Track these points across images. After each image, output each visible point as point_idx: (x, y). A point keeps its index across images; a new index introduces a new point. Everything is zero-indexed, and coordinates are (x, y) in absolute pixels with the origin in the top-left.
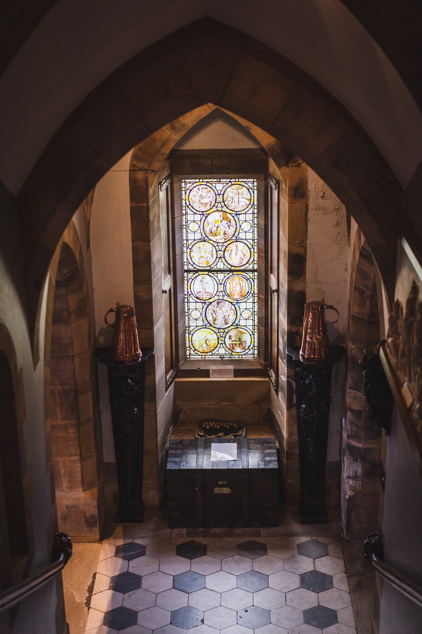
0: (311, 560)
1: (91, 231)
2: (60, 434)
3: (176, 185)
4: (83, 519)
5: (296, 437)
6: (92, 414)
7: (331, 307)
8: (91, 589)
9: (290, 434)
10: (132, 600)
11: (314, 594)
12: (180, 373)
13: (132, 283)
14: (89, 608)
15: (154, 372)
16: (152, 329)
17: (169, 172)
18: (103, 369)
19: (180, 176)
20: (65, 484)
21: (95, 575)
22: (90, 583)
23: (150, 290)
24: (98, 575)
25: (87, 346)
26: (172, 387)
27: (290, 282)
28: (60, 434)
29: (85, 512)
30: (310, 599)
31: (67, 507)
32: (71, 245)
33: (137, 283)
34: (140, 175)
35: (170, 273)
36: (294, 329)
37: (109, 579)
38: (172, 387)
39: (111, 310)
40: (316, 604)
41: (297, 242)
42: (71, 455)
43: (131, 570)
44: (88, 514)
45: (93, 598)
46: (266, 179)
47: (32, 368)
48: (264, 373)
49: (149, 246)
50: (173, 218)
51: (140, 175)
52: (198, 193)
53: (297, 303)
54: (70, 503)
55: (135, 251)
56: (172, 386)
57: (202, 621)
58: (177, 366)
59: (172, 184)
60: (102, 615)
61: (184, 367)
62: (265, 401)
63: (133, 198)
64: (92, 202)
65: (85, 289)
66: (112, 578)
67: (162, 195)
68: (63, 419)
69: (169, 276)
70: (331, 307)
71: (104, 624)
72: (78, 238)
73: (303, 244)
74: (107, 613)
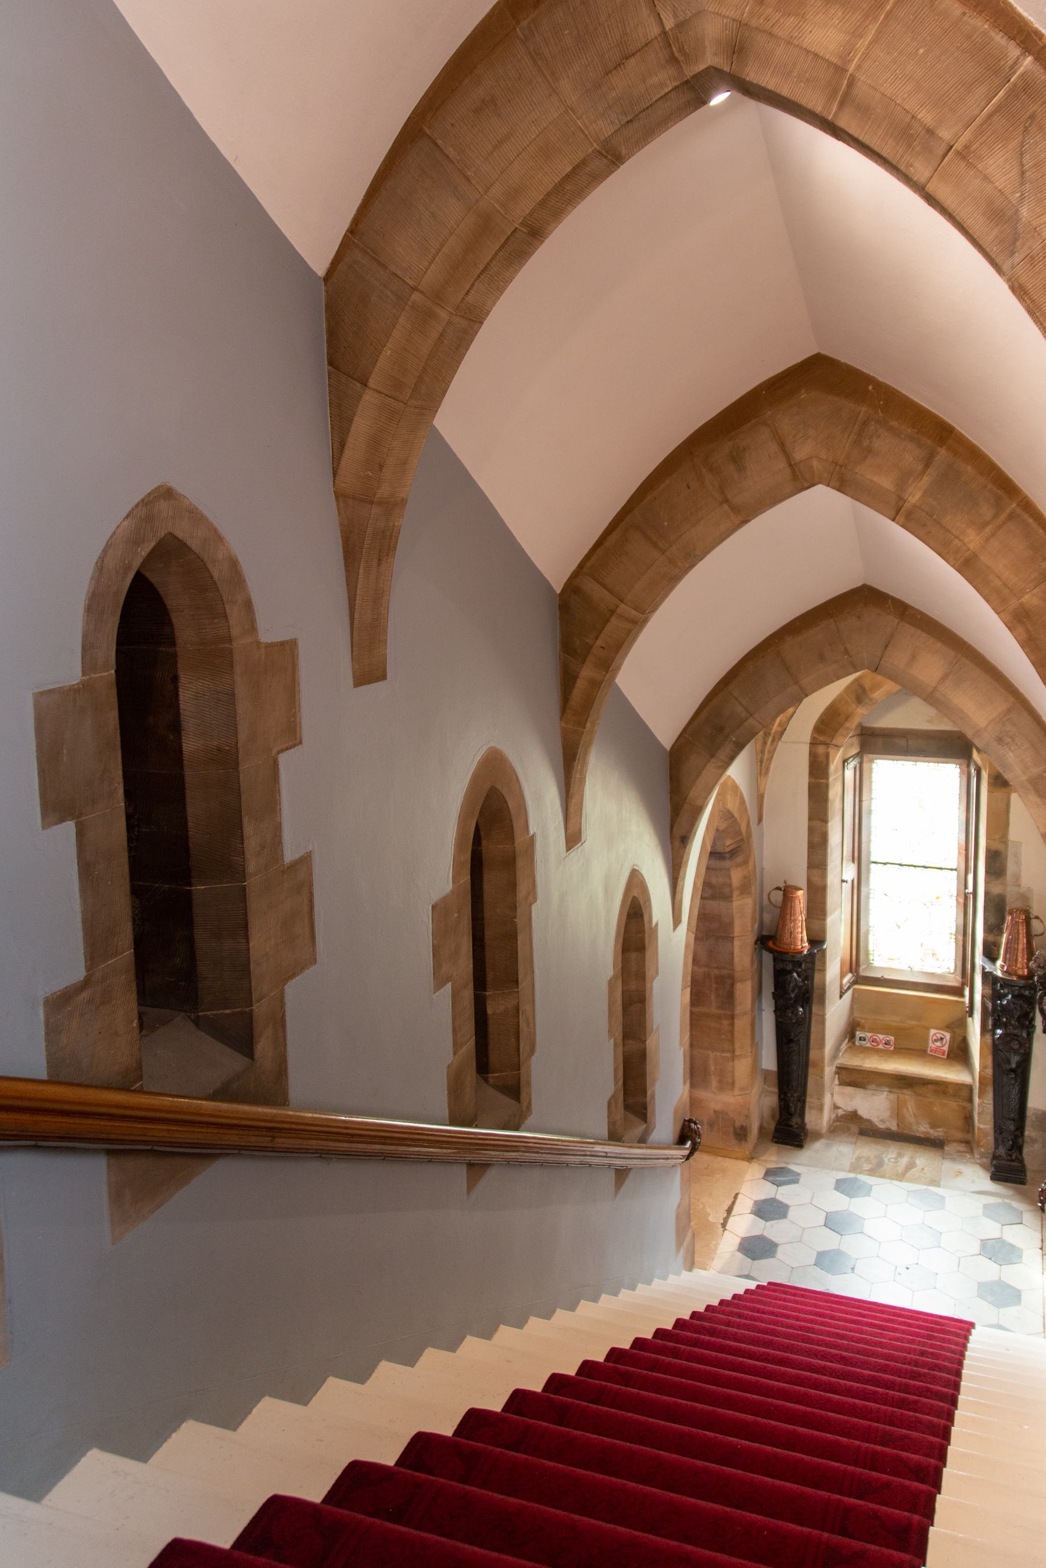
0: (999, 1226)
1: (765, 805)
2: (713, 1025)
3: (865, 765)
4: (732, 1130)
5: (989, 1071)
6: (749, 1006)
7: (1037, 918)
8: (729, 1211)
9: (983, 1067)
10: (773, 1230)
11: (996, 1266)
12: (859, 980)
13: (806, 866)
14: (725, 1230)
15: (823, 970)
16: (824, 919)
17: (858, 750)
18: (768, 958)
19: (870, 756)
20: (714, 1083)
21: (737, 1195)
22: (729, 1203)
23: (824, 876)
24: (740, 1196)
25: (750, 929)
26: (848, 996)
27: (986, 882)
28: (713, 1025)
29: (734, 1122)
30: (990, 1270)
31: (715, 1111)
32: (736, 815)
33: (811, 866)
34: (821, 750)
35: (853, 861)
36: (991, 938)
37: (752, 1202)
38: (848, 996)
39: (778, 888)
40: (996, 1278)
41: (997, 837)
42: (723, 1051)
43: (779, 1197)
44: (738, 1124)
45: (731, 1220)
46: (968, 766)
47: (672, 927)
48: (958, 991)
49: (826, 827)
50: (860, 801)
51: (821, 750)
52: (888, 773)
53: (997, 908)
54: (718, 1107)
55: (811, 831)
56: (850, 992)
57: (853, 1269)
58: (857, 971)
59: (861, 763)
60: (738, 1241)
61: (863, 972)
62: (958, 1027)
63: (812, 774)
64: (767, 773)
65: (751, 864)
66: (756, 1202)
67: (849, 774)
68: (718, 1008)
69: (852, 865)
70: (1037, 918)
71: (739, 1250)
72: (746, 809)
73: (1004, 838)
74: (743, 1239)
